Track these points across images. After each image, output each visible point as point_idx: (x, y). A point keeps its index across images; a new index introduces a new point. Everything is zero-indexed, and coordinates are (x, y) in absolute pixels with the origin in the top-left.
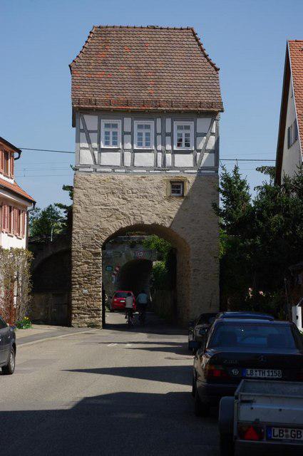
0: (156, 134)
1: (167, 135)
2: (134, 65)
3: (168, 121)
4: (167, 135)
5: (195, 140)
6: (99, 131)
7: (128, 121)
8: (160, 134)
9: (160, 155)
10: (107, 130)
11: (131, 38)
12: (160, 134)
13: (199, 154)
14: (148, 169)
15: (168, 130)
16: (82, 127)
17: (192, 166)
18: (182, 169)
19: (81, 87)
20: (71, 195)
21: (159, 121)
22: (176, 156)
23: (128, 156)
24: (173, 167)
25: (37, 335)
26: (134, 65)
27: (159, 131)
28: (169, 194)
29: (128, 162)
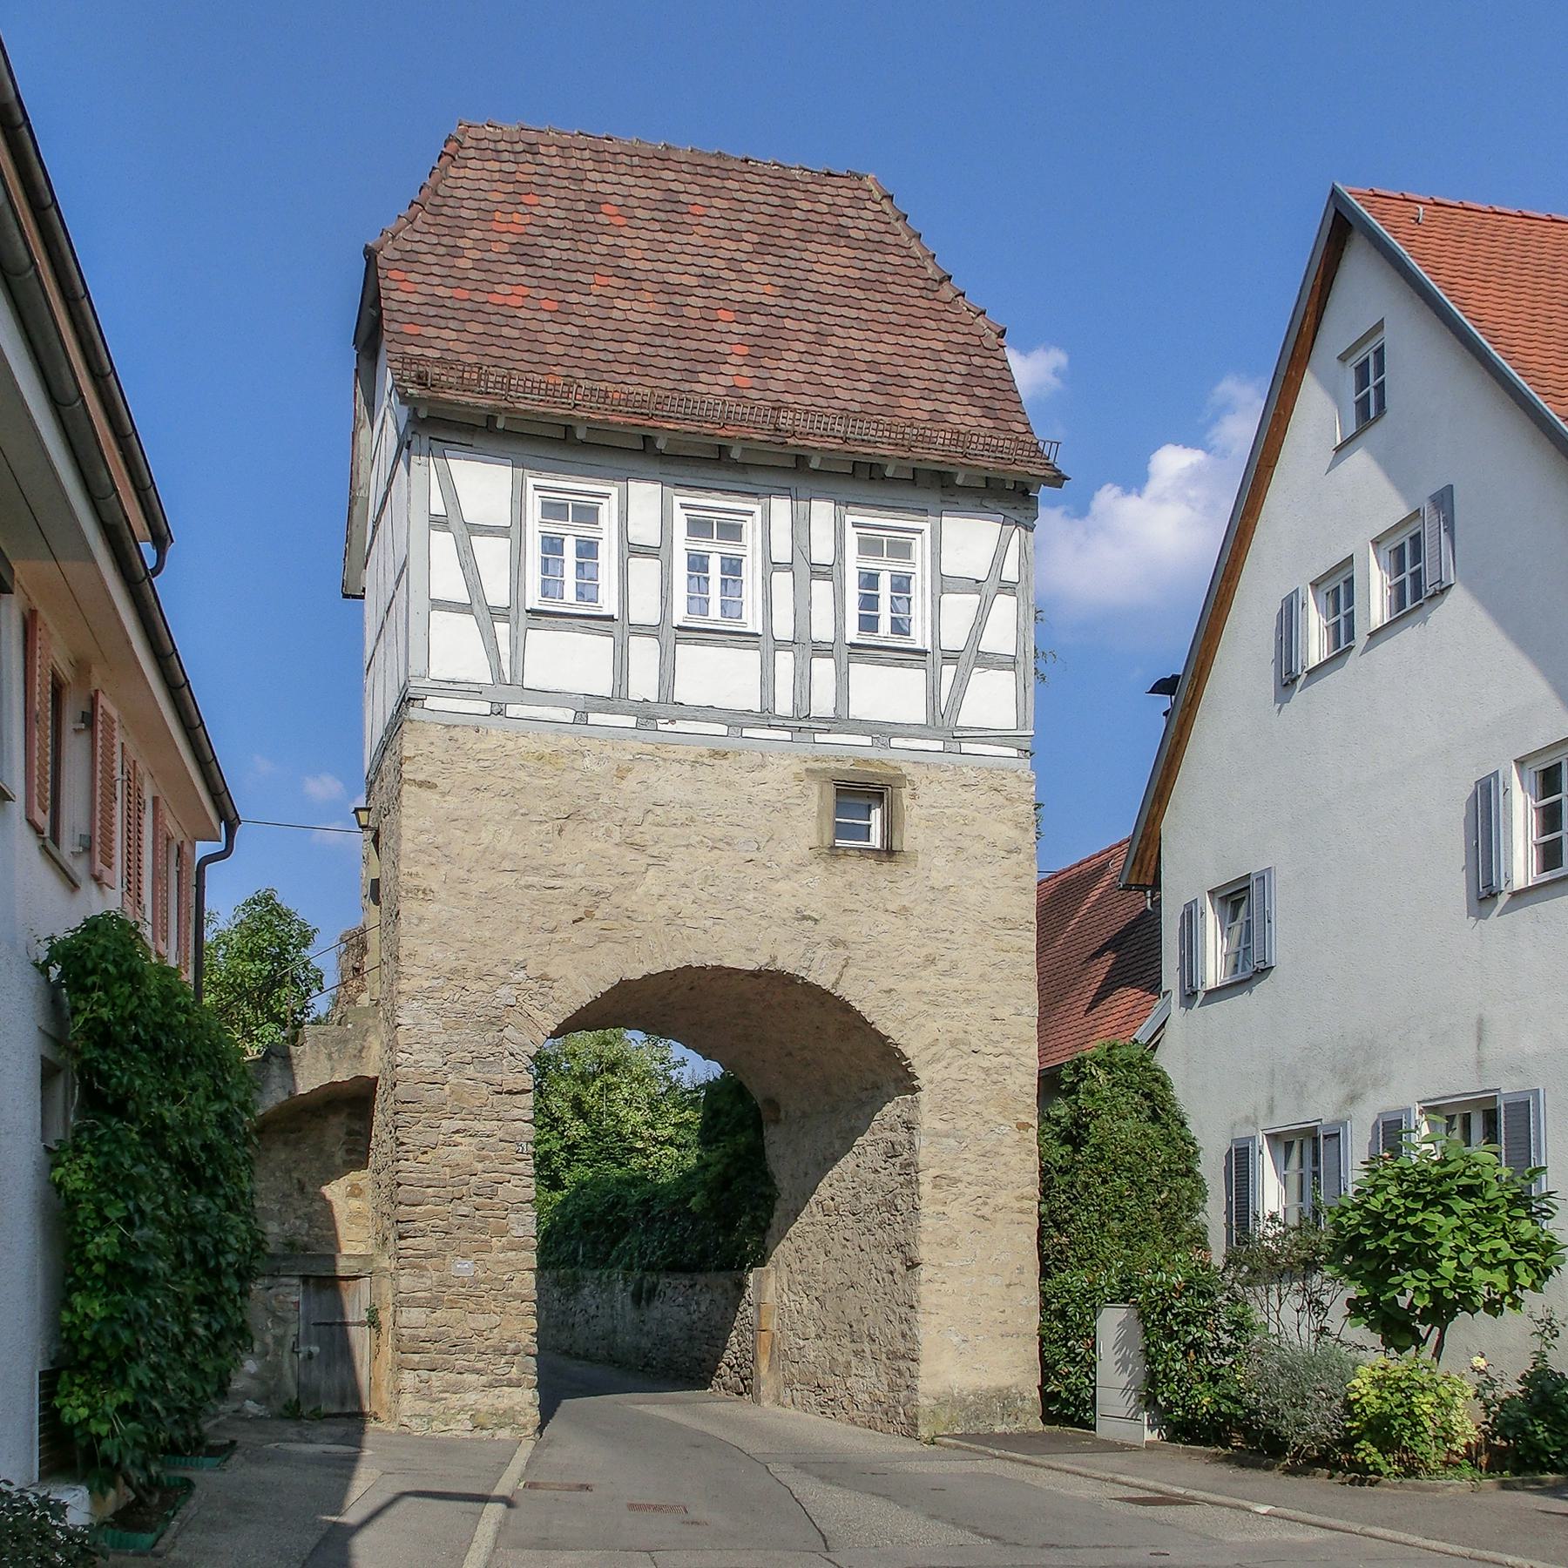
0: (772, 566)
1: (819, 572)
2: (653, 276)
3: (404, 985)
4: (819, 572)
5: (937, 605)
6: (512, 532)
7: (645, 496)
8: (789, 567)
9: (785, 661)
10: (554, 528)
11: (630, 181)
12: (789, 567)
13: (949, 671)
14: (736, 719)
15: (822, 552)
16: (438, 507)
17: (919, 716)
18: (882, 731)
19: (431, 332)
20: (376, 841)
21: (781, 507)
22: (859, 672)
23: (643, 653)
24: (840, 721)
25: (1181, 969)
26: (653, 276)
27: (782, 552)
28: (827, 841)
29: (643, 685)
